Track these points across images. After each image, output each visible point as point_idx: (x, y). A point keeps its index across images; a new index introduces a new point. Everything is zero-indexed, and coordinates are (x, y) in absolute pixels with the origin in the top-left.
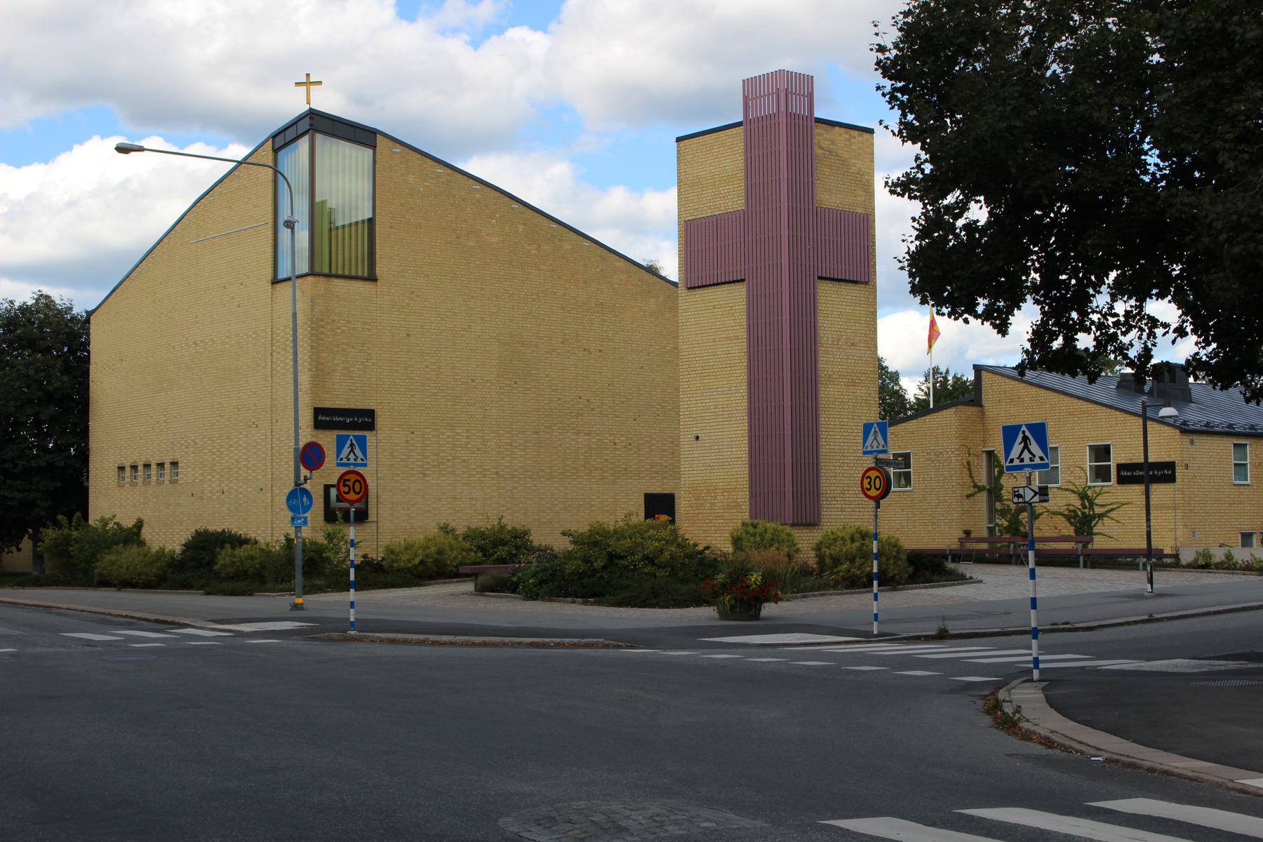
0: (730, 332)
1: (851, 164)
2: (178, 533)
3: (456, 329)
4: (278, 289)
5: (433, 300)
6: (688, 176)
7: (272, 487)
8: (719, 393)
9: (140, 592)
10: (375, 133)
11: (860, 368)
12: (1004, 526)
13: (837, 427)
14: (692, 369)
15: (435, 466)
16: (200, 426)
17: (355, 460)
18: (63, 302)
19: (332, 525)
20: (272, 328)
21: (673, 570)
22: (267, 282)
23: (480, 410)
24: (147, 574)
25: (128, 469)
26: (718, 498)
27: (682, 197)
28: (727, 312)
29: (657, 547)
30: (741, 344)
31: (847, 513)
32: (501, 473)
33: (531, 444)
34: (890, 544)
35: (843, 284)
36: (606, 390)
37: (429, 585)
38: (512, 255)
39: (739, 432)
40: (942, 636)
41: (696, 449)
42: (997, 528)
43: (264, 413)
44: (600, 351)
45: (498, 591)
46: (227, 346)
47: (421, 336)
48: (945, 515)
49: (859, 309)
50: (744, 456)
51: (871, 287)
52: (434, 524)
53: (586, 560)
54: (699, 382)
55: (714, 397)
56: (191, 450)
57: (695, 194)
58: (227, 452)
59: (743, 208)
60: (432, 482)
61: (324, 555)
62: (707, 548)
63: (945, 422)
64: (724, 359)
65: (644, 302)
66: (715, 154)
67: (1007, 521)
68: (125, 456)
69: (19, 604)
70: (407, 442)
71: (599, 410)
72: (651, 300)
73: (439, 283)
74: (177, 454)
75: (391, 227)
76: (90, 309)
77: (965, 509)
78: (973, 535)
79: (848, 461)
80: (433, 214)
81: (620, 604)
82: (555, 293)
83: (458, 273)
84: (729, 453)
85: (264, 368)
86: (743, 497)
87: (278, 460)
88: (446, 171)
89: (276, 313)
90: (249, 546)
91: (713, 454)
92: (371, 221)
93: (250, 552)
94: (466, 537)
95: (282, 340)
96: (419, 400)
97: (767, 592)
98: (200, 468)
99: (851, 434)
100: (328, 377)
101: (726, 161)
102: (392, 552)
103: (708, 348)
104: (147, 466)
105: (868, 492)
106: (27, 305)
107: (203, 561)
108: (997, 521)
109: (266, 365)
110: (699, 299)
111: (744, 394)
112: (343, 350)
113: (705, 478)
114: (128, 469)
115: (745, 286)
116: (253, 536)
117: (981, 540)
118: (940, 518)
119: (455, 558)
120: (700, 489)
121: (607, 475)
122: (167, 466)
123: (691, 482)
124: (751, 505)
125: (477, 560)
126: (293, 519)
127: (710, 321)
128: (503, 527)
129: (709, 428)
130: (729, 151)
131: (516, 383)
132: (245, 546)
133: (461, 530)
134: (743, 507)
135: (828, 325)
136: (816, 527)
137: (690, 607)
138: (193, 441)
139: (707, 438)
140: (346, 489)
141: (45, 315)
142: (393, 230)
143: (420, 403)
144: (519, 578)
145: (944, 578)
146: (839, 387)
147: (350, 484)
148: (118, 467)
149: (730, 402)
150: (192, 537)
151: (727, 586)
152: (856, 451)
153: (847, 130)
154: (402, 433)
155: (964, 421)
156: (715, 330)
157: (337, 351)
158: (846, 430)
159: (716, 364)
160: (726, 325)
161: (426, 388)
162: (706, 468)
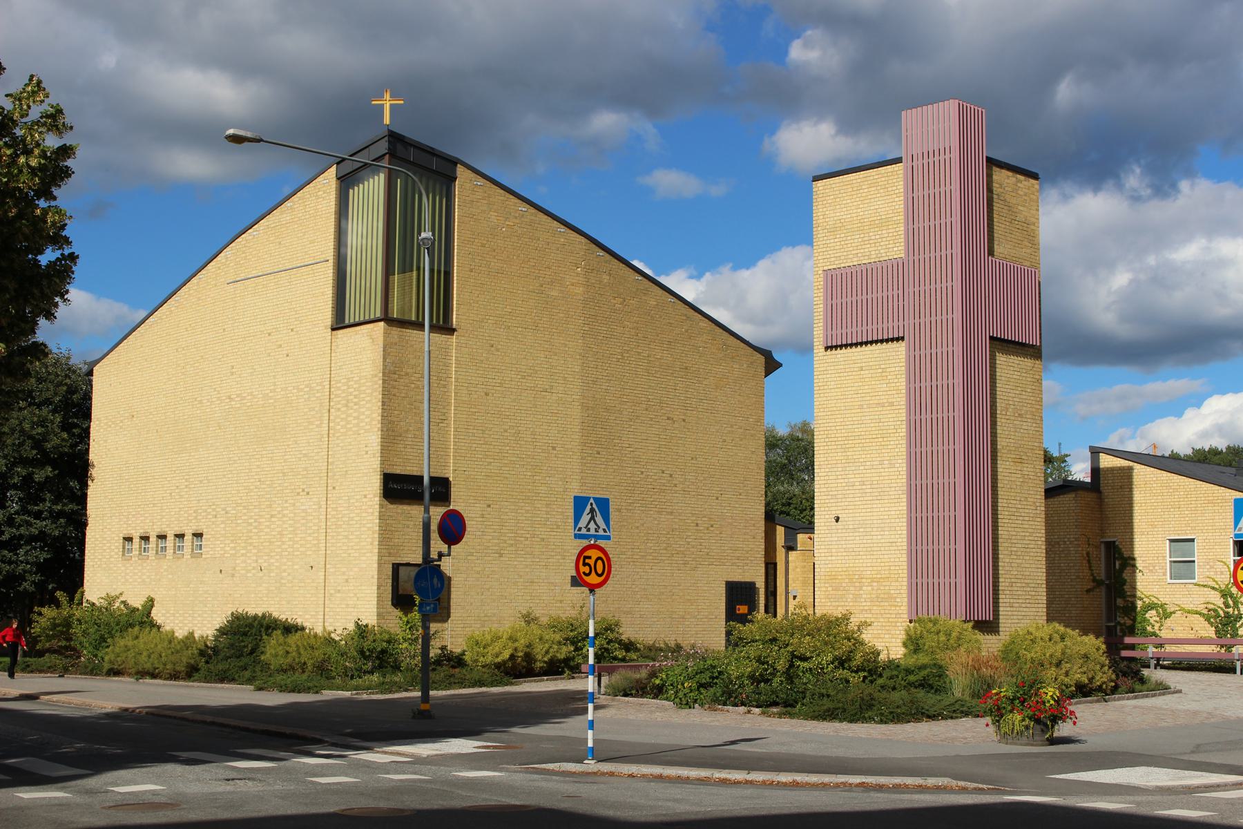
0: (883, 397)
2: (199, 616)
4: (339, 336)
6: (827, 220)
8: (866, 467)
14: (830, 440)
15: (512, 545)
16: (233, 492)
17: (596, 531)
23: (560, 483)
26: (864, 588)
42: (1118, 628)
44: (684, 420)
45: (631, 695)
55: (860, 472)
57: (836, 240)
58: (268, 523)
59: (903, 255)
64: (873, 429)
66: (864, 194)
68: (133, 525)
71: (681, 486)
74: (201, 524)
81: (816, 717)
84: (879, 537)
87: (335, 534)
91: (858, 538)
96: (496, 468)
101: (879, 203)
108: (1118, 619)
110: (842, 359)
113: (847, 565)
127: (857, 384)
129: (853, 507)
130: (882, 191)
133: (544, 620)
139: (850, 519)
140: (587, 569)
147: (591, 562)
148: (124, 538)
159: (863, 433)
160: (877, 390)
162: (848, 554)
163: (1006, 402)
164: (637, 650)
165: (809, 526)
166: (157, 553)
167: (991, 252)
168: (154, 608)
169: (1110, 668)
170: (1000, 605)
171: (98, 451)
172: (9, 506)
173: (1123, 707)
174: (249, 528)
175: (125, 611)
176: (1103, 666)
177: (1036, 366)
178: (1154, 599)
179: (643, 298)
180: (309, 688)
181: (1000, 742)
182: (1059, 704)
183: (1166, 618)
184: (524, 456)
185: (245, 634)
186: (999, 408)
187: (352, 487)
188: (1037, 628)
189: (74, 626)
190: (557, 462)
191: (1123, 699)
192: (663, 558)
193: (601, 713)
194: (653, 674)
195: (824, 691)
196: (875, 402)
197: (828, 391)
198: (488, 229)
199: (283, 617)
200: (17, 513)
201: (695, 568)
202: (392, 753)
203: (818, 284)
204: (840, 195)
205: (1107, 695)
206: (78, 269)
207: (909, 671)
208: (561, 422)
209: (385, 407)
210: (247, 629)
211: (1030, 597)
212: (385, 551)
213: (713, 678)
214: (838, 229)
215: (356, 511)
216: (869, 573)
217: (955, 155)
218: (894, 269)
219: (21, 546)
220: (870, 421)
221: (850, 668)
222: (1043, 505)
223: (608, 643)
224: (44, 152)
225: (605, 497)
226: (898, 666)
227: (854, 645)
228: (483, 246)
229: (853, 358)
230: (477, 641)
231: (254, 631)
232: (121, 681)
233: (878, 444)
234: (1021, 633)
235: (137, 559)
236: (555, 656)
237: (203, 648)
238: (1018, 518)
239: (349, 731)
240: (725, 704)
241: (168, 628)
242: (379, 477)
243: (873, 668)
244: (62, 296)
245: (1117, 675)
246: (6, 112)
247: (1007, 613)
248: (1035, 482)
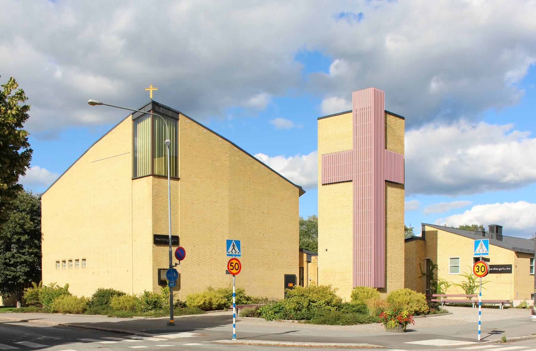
8: (338, 230)
17: (235, 253)
18: (28, 190)
23: (221, 237)
35: (393, 184)
42: (430, 291)
44: (268, 213)
55: (335, 232)
59: (352, 149)
66: (337, 125)
70: (192, 250)
82: (251, 188)
84: (342, 257)
100: (159, 221)
105: (477, 273)
108: (430, 288)
110: (328, 189)
113: (330, 267)
131: (236, 226)
133: (216, 289)
147: (234, 265)
159: (336, 217)
164: (251, 300)
165: (316, 253)
166: (69, 267)
167: (386, 148)
168: (69, 288)
169: (427, 305)
170: (387, 282)
171: (45, 229)
172: (12, 251)
173: (431, 319)
175: (58, 289)
176: (424, 304)
177: (402, 192)
178: (443, 280)
179: (252, 166)
180: (128, 316)
181: (386, 331)
182: (408, 317)
183: (448, 287)
184: (207, 227)
185: (103, 296)
186: (388, 208)
188: (401, 290)
189: (39, 295)
190: (220, 230)
191: (431, 316)
192: (261, 266)
193: (238, 323)
194: (257, 309)
195: (321, 314)
198: (192, 139)
199: (117, 290)
200: (15, 253)
201: (273, 270)
202: (160, 338)
203: (320, 160)
205: (426, 315)
206: (33, 155)
207: (353, 306)
209: (154, 209)
210: (104, 294)
211: (398, 279)
212: (155, 264)
213: (280, 309)
214: (327, 138)
216: (338, 270)
217: (373, 109)
218: (350, 154)
219: (18, 266)
221: (331, 305)
222: (404, 245)
223: (240, 298)
224: (18, 108)
225: (239, 240)
226: (349, 305)
227: (333, 297)
228: (190, 146)
230: (191, 297)
231: (107, 295)
232: (58, 315)
234: (395, 292)
235: (61, 269)
236: (220, 303)
237: (88, 302)
238: (395, 249)
239: (144, 330)
240: (284, 319)
241: (74, 295)
242: (152, 236)
243: (339, 306)
244: (27, 166)
245: (430, 308)
246: (2, 93)
247: (389, 285)
248: (401, 236)
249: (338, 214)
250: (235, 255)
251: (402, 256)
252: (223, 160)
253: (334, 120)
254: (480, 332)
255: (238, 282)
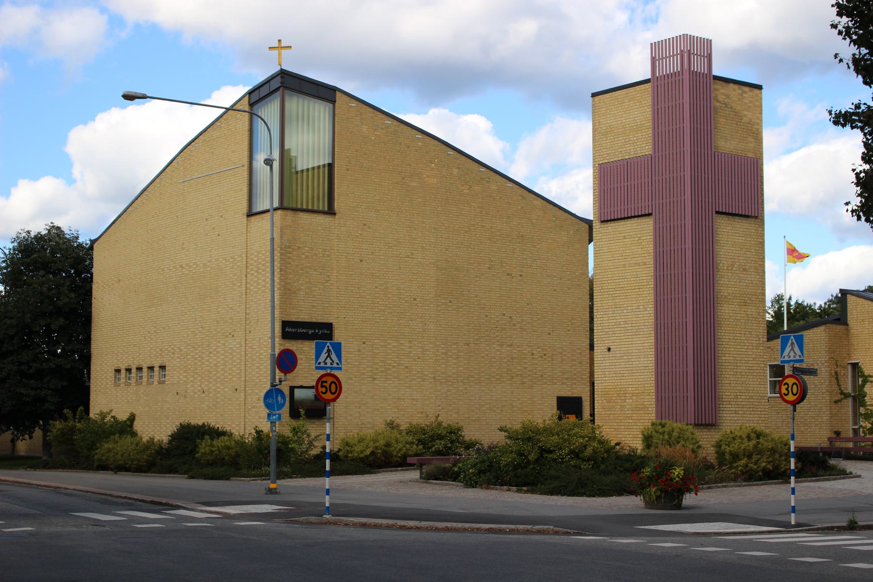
0: (639, 259)
1: (743, 115)
3: (401, 256)
4: (252, 221)
5: (382, 231)
6: (601, 126)
7: (245, 388)
8: (628, 311)
9: (133, 475)
10: (335, 90)
11: (751, 291)
12: (868, 428)
13: (731, 341)
14: (604, 290)
16: (185, 335)
17: (331, 364)
18: (72, 232)
19: (296, 420)
20: (247, 254)
21: (596, 463)
22: (243, 215)
23: (420, 325)
24: (138, 460)
25: (123, 372)
26: (627, 401)
27: (596, 144)
28: (636, 242)
29: (582, 443)
30: (648, 269)
31: (740, 416)
32: (437, 378)
33: (462, 354)
34: (782, 442)
35: (737, 218)
36: (526, 309)
37: (379, 472)
38: (448, 194)
39: (646, 344)
40: (852, 527)
41: (608, 358)
42: (861, 430)
43: (239, 325)
44: (521, 276)
45: (441, 479)
46: (209, 269)
47: (371, 261)
48: (816, 418)
49: (750, 239)
50: (651, 365)
51: (760, 221)
52: (382, 421)
53: (520, 454)
54: (610, 301)
55: (624, 314)
56: (176, 355)
57: (607, 141)
59: (650, 153)
60: (380, 384)
61: (290, 446)
62: (618, 444)
63: (815, 338)
64: (633, 282)
65: (557, 235)
66: (626, 107)
67: (870, 423)
68: (121, 360)
69: (32, 484)
70: (359, 351)
71: (519, 325)
72: (563, 233)
73: (387, 217)
74: (164, 359)
75: (348, 170)
76: (93, 238)
77: (834, 413)
78: (842, 435)
79: (740, 371)
80: (382, 159)
83: (403, 208)
84: (637, 363)
85: (240, 287)
86: (650, 400)
87: (251, 365)
88: (394, 123)
89: (250, 241)
90: (226, 438)
91: (623, 364)
92: (331, 166)
93: (226, 443)
94: (409, 432)
95: (255, 264)
96: (369, 315)
97: (688, 484)
98: (185, 371)
99: (743, 347)
100: (294, 295)
101: (636, 113)
102: (347, 444)
103: (619, 272)
104: (139, 369)
105: (786, 397)
106: (41, 235)
107: (187, 450)
108: (861, 423)
109: (241, 285)
110: (611, 231)
111: (651, 312)
112: (307, 272)
113: (616, 384)
114: (123, 372)
115: (652, 219)
116: (228, 429)
117: (848, 440)
118: (812, 420)
119: (400, 450)
120: (611, 393)
121: (526, 380)
122: (156, 369)
123: (603, 387)
124: (657, 407)
125: (419, 452)
126: (269, 415)
127: (621, 249)
128: (440, 424)
129: (619, 341)
130: (638, 104)
131: (450, 302)
132: (222, 438)
134: (650, 409)
135: (724, 253)
136: (714, 427)
137: (612, 496)
138: (179, 348)
139: (618, 349)
140: (324, 390)
141: (56, 242)
142: (349, 172)
143: (371, 318)
144: (459, 468)
145: (828, 473)
146: (733, 306)
147: (327, 385)
149: (639, 319)
150: (177, 429)
151: (653, 479)
152: (748, 362)
153: (740, 86)
154: (355, 343)
155: (832, 337)
156: (626, 257)
157: (302, 273)
158: (739, 344)
159: (626, 286)
160: (635, 253)
161: (375, 305)
162: (617, 375)
163: (733, 260)
174: (196, 361)
187: (262, 331)
196: (634, 262)
197: (603, 254)
204: (610, 108)
208: (420, 280)
215: (264, 349)
218: (650, 162)
220: (630, 277)
229: (619, 229)
233: (636, 293)
249: (629, 280)
250: (332, 368)
251: (761, 359)
252: (425, 176)
253: (619, 97)
254: (794, 510)
255: (456, 412)
